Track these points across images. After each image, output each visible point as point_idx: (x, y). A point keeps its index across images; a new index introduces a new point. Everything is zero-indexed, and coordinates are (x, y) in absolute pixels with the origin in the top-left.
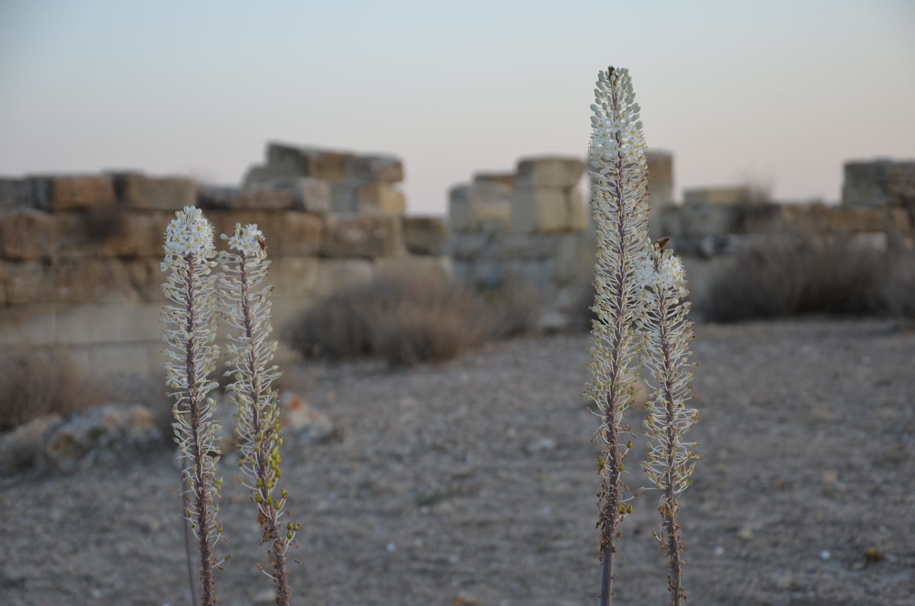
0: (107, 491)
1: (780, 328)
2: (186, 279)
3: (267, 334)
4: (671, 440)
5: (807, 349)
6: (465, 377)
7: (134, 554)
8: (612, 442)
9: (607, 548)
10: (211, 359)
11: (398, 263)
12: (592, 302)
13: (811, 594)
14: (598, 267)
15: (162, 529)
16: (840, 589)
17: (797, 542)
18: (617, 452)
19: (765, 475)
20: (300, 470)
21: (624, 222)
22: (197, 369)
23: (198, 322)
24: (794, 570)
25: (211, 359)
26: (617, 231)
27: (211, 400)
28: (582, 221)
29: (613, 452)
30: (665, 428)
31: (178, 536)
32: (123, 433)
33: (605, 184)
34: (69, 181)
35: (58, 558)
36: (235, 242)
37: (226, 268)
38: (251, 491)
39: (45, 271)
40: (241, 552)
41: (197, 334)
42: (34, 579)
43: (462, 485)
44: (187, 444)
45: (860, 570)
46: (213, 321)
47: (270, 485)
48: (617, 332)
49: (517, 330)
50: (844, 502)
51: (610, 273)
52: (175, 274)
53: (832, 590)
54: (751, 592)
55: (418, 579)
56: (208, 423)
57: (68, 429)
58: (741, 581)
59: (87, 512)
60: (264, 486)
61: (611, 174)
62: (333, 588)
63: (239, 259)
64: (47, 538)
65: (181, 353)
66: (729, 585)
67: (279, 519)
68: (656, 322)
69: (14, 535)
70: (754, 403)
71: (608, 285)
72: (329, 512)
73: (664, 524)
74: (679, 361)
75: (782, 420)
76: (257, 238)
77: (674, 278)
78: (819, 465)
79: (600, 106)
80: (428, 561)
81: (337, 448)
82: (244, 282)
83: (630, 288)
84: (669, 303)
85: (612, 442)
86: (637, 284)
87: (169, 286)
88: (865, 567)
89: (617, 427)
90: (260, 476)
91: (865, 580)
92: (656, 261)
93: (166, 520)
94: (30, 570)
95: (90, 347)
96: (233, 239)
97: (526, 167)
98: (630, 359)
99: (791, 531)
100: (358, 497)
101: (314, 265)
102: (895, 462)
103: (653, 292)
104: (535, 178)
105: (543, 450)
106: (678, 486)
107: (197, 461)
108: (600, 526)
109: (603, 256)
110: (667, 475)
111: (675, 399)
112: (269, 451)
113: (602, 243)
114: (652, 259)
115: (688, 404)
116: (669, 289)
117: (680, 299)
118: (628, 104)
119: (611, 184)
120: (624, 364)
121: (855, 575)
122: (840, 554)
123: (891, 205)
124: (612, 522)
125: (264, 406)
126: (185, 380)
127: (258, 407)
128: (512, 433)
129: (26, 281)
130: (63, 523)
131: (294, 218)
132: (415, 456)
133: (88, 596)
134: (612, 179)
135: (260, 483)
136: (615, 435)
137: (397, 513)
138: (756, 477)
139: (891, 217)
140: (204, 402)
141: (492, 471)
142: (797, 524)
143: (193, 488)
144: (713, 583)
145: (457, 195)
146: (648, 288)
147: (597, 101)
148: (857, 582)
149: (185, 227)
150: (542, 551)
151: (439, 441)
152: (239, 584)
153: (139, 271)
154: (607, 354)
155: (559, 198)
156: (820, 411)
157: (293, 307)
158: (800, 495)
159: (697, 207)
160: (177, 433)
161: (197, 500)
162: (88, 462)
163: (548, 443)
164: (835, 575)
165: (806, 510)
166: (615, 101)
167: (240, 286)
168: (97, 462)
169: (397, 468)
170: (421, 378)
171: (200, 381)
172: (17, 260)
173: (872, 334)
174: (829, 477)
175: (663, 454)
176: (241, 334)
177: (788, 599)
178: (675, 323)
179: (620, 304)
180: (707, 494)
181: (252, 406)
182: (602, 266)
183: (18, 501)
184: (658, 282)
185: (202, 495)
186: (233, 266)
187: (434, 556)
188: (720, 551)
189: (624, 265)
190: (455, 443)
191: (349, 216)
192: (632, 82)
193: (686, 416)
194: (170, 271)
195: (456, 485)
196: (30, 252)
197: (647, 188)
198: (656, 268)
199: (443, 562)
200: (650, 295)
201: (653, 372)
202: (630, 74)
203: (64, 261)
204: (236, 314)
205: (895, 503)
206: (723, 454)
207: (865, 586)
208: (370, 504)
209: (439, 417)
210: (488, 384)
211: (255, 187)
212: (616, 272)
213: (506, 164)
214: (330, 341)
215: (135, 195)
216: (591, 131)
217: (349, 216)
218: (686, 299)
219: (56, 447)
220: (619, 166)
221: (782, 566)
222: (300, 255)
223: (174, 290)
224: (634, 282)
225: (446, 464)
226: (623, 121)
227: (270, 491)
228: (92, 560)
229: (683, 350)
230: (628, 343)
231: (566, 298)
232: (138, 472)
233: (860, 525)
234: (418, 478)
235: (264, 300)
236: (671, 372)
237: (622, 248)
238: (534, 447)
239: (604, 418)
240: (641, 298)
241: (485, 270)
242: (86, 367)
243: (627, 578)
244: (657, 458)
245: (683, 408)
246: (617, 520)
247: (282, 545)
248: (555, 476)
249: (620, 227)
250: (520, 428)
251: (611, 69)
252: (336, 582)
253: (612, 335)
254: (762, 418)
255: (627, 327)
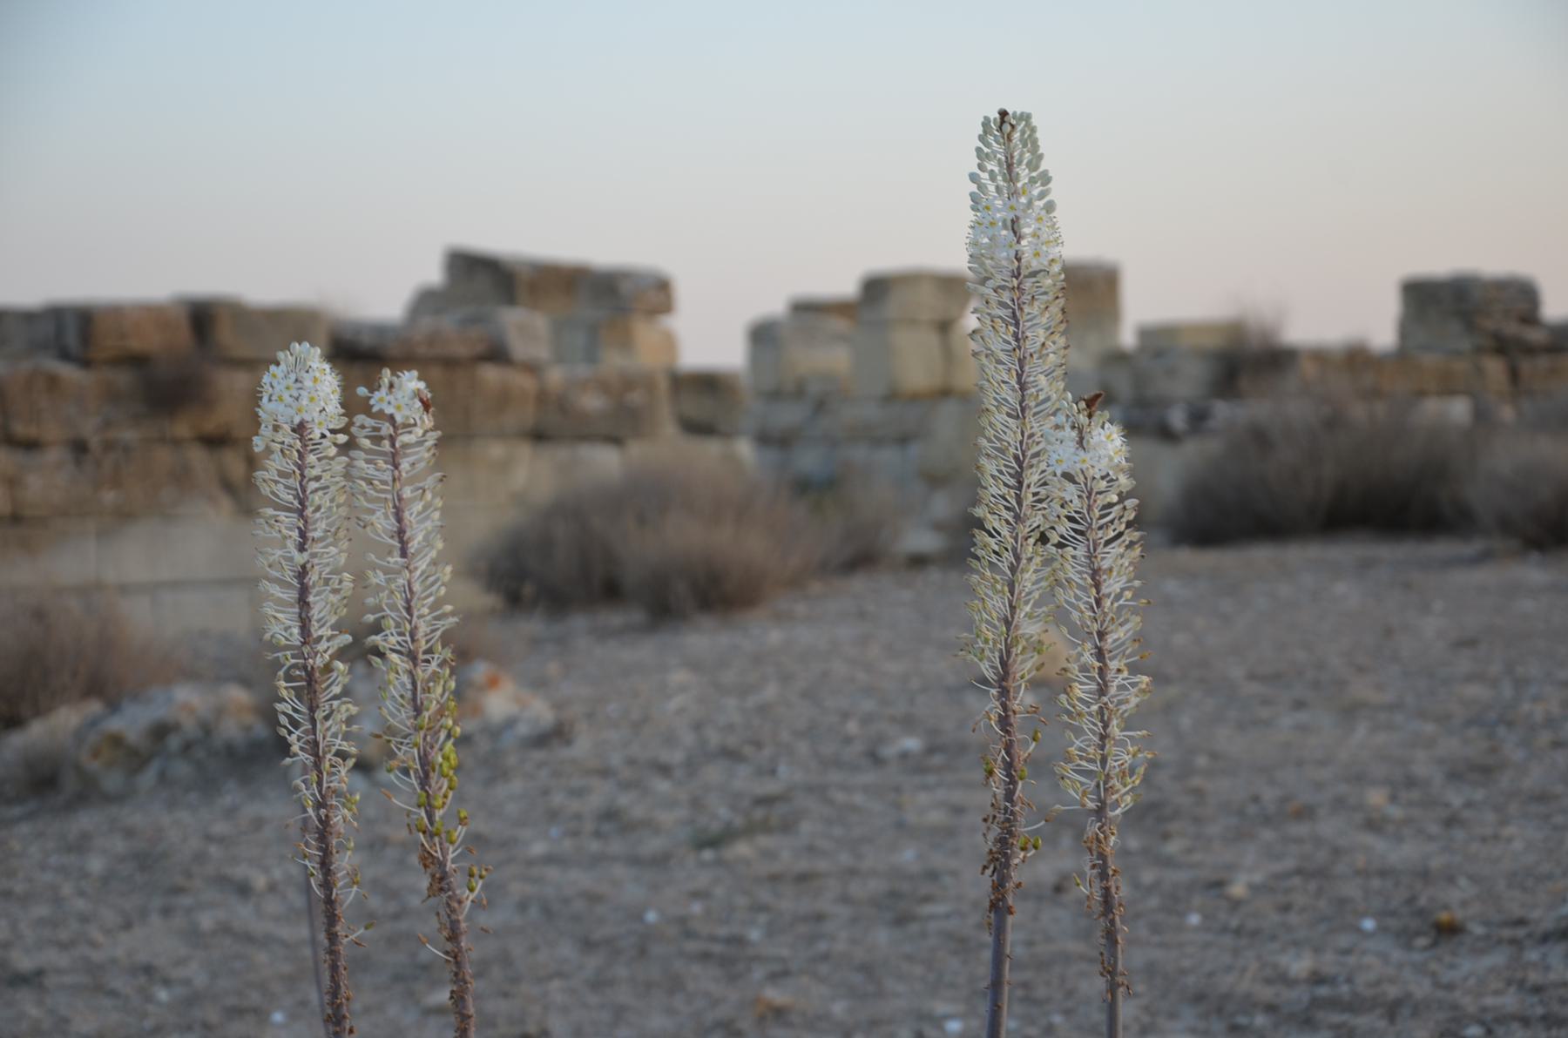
0: (181, 826)
1: (1301, 555)
2: (296, 464)
3: (433, 554)
4: (1106, 726)
5: (1341, 588)
6: (775, 636)
7: (225, 929)
8: (1007, 732)
9: (999, 907)
10: (338, 597)
11: (665, 447)
12: (976, 502)
13: (1344, 989)
14: (984, 442)
15: (272, 888)
16: (1392, 981)
17: (1322, 904)
18: (1016, 749)
19: (1269, 795)
20: (501, 791)
21: (1026, 368)
22: (315, 613)
23: (317, 534)
24: (1317, 950)
25: (338, 597)
26: (1013, 382)
27: (340, 665)
28: (966, 378)
29: (1008, 748)
30: (1095, 708)
31: (298, 901)
32: (207, 729)
33: (993, 304)
34: (116, 312)
35: (98, 936)
36: (381, 400)
37: (366, 443)
38: (409, 813)
39: (78, 463)
40: (403, 925)
41: (314, 555)
42: (59, 971)
43: (769, 814)
44: (299, 739)
45: (1425, 949)
46: (341, 534)
47: (438, 802)
48: (1014, 550)
49: (862, 558)
50: (1399, 839)
51: (1002, 451)
52: (277, 456)
53: (1378, 983)
54: (1245, 986)
55: (696, 969)
56: (335, 703)
57: (115, 724)
58: (1229, 969)
59: (146, 860)
60: (430, 805)
61: (1003, 288)
62: (555, 984)
63: (386, 429)
64: (80, 904)
65: (289, 586)
66: (1211, 974)
67: (453, 861)
68: (1082, 533)
69: (26, 900)
70: (1252, 677)
71: (1001, 472)
72: (550, 859)
73: (1094, 867)
74: (1118, 597)
75: (1299, 705)
76: (417, 394)
77: (1111, 459)
78: (1359, 779)
79: (985, 176)
80: (713, 939)
81: (565, 753)
82: (396, 466)
83: (1036, 477)
84: (1101, 500)
85: (1007, 732)
86: (1050, 470)
87: (266, 475)
88: (1434, 944)
89: (1016, 707)
90: (423, 788)
91: (1433, 966)
92: (1080, 431)
93: (277, 874)
94: (51, 957)
95: (152, 589)
96: (377, 395)
97: (876, 288)
98: (1036, 595)
99: (1313, 886)
100: (598, 834)
101: (524, 451)
102: (1484, 771)
103: (1075, 482)
104: (893, 307)
105: (904, 756)
106: (1116, 804)
107: (317, 765)
108: (989, 872)
109: (991, 424)
110: (1098, 786)
111: (1111, 659)
112: (437, 747)
113: (989, 403)
114: (1073, 427)
115: (1134, 669)
116: (1103, 478)
117: (1120, 495)
118: (1032, 170)
119: (1003, 305)
120: (1026, 603)
121: (1417, 957)
122: (1393, 923)
123: (1479, 350)
124: (1007, 865)
125: (430, 671)
126: (296, 631)
127: (420, 674)
128: (852, 727)
129: (47, 479)
130: (105, 880)
131: (491, 374)
132: (691, 766)
133: (149, 998)
134: (1006, 297)
135: (423, 799)
136: (1012, 720)
137: (661, 861)
138: (1256, 799)
139: (1480, 371)
140: (328, 669)
141: (819, 791)
142: (1322, 873)
143: (310, 810)
144: (1183, 972)
145: (762, 335)
146: (1068, 476)
147: (981, 167)
148: (1420, 969)
149: (293, 377)
150: (901, 921)
151: (732, 741)
152: (398, 978)
153: (233, 462)
154: (999, 587)
155: (932, 339)
156: (1361, 689)
157: (487, 521)
158: (1329, 827)
159: (1159, 354)
160: (284, 720)
161: (319, 831)
162: (148, 778)
163: (912, 743)
164: (1384, 957)
165: (1337, 852)
166: (1010, 166)
167: (389, 473)
168: (163, 778)
169: (662, 786)
170: (702, 638)
171: (320, 633)
172: (31, 445)
173: (1448, 564)
174: (1376, 797)
175: (1091, 750)
176: (390, 553)
177: (1306, 998)
178: (1112, 534)
179: (1020, 503)
180: (1173, 827)
181: (411, 673)
182: (990, 441)
183: (32, 843)
184: (1084, 466)
185: (325, 822)
186: (377, 440)
187: (723, 931)
188: (1194, 919)
189: (1026, 438)
190: (758, 745)
191: (582, 371)
192: (1038, 135)
193: (1131, 691)
194: (268, 451)
195: (759, 813)
196: (51, 431)
197: (1063, 311)
198: (1081, 442)
199: (738, 941)
200: (1071, 487)
201: (1075, 615)
202: (1034, 121)
203: (109, 446)
204: (382, 522)
205: (1484, 840)
206: (1202, 761)
207: (1433, 974)
208: (616, 846)
209: (731, 703)
210: (811, 644)
211: (427, 323)
212: (1012, 450)
213: (845, 286)
214: (553, 578)
215: (227, 336)
216: (971, 216)
217: (582, 371)
218: (1130, 495)
219: (96, 754)
220: (1016, 274)
221: (1296, 944)
222: (501, 435)
223: (276, 482)
224: (1043, 466)
225: (744, 780)
226: (1023, 200)
227: (439, 814)
228: (155, 941)
229: (1124, 579)
230: (1032, 567)
231: (942, 505)
232: (231, 794)
233: (1425, 875)
234: (696, 803)
235: (429, 496)
236: (1105, 614)
237: (1023, 410)
238: (889, 751)
239: (994, 691)
240: (1056, 493)
241: (809, 460)
242: (142, 620)
243: (1042, 965)
244: (1081, 758)
245: (1126, 674)
246: (1016, 861)
247: (460, 902)
248: (923, 798)
249: (1019, 376)
250: (867, 720)
251: (1003, 114)
252: (560, 975)
253: (1006, 554)
254: (1266, 702)
255: (1032, 541)
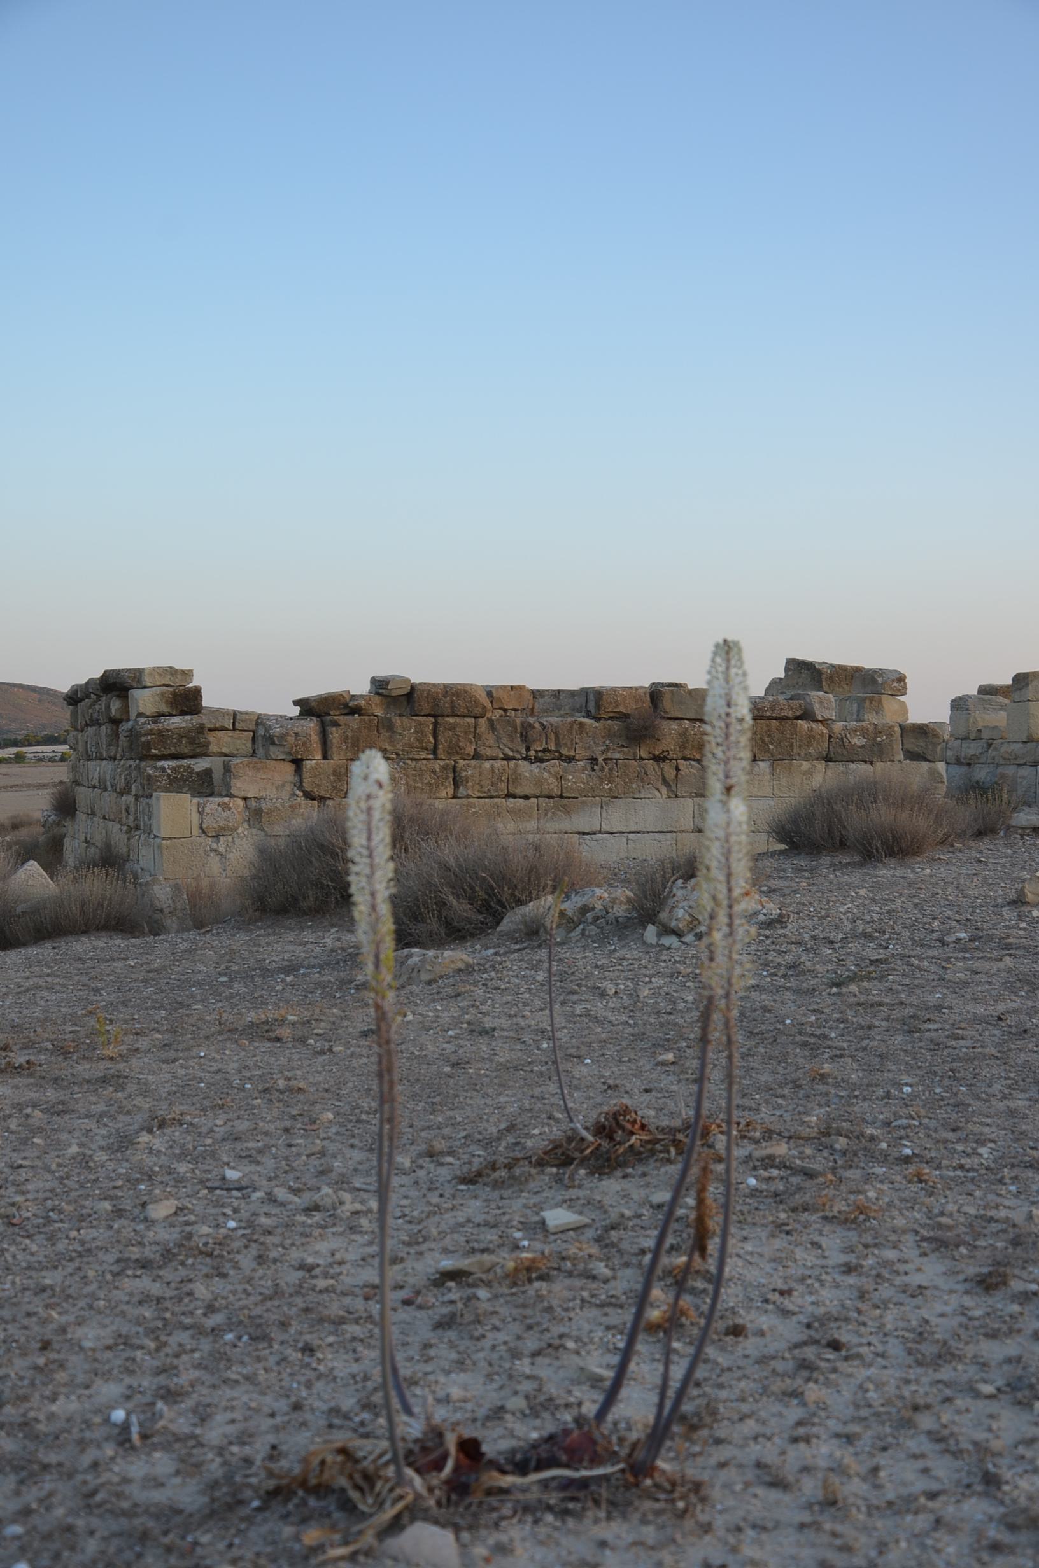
7: (587, 1014)
43: (878, 969)
100: (785, 976)
101: (821, 766)
104: (1030, 692)
145: (959, 705)
170: (887, 871)
172: (570, 759)
196: (580, 753)
208: (792, 983)
214: (806, 837)
215: (666, 703)
241: (981, 774)
251: (725, 641)
